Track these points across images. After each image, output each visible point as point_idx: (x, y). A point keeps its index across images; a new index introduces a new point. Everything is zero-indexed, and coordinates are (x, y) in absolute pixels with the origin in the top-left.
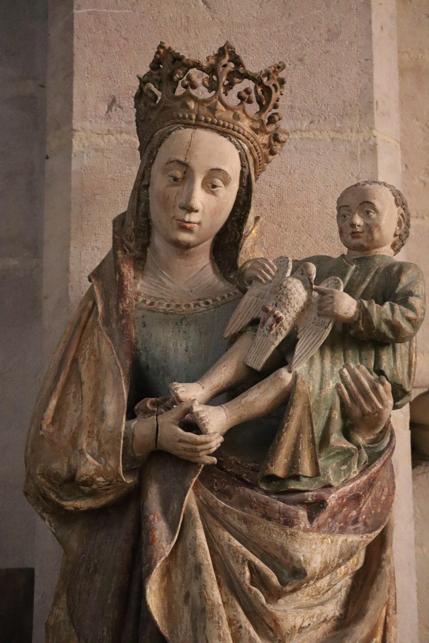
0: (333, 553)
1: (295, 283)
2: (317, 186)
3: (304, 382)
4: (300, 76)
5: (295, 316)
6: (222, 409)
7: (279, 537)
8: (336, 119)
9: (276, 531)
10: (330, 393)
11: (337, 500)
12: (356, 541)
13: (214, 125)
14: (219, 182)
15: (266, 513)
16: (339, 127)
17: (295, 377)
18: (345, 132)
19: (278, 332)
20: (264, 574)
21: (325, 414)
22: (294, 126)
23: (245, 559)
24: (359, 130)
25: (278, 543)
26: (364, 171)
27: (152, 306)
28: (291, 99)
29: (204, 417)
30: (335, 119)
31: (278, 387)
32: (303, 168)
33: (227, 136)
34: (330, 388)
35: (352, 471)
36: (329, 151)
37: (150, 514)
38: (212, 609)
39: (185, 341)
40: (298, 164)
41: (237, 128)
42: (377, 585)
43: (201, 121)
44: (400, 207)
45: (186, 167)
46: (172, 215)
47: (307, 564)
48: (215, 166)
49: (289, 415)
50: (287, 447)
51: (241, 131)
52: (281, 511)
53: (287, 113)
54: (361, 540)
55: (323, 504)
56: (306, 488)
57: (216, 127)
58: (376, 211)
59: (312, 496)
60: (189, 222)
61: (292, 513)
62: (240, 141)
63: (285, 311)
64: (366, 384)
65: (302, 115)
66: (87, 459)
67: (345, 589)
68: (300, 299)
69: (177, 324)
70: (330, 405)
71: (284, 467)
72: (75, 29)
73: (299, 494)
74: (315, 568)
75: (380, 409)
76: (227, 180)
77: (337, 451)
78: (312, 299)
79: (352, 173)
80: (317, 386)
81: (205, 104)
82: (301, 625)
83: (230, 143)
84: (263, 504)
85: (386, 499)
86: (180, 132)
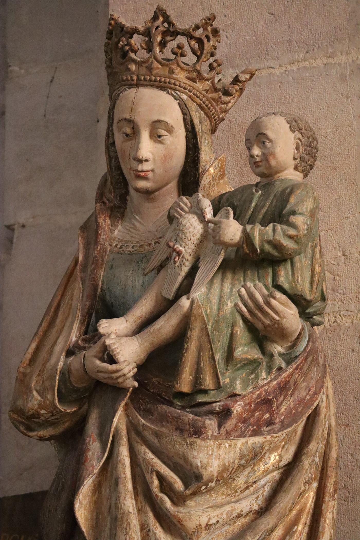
0: (232, 456)
1: (189, 219)
2: (312, 111)
3: (199, 306)
4: (297, 11)
5: (194, 248)
6: (136, 339)
7: (181, 447)
8: (328, 46)
9: (179, 443)
10: (229, 312)
11: (243, 407)
12: (259, 442)
13: (152, 82)
14: (162, 132)
15: (179, 426)
16: (331, 52)
17: (192, 303)
18: (336, 56)
19: (182, 263)
20: (169, 481)
21: (226, 331)
22: (292, 58)
23: (153, 470)
24: (348, 52)
25: (180, 452)
26: (353, 90)
27: (121, 249)
28: (290, 34)
29: (115, 348)
30: (327, 45)
31: (179, 313)
32: (300, 96)
33: (166, 90)
34: (229, 307)
35: (260, 379)
36: (322, 76)
37: (87, 437)
38: (123, 518)
39: (142, 277)
40: (296, 93)
41: (173, 81)
42: (292, 479)
43: (141, 80)
44: (297, 132)
45: (132, 124)
46: (129, 167)
47: (203, 468)
48: (156, 118)
49: (187, 338)
50: (190, 366)
51: (177, 83)
52: (191, 422)
53: (286, 48)
54: (264, 440)
55: (230, 412)
56: (213, 400)
57: (154, 83)
58: (271, 141)
59: (220, 406)
60: (143, 171)
61: (200, 424)
62: (178, 92)
63: (184, 244)
64: (260, 299)
65: (299, 47)
66: (33, 395)
67: (270, 484)
68: (196, 232)
69: (138, 262)
70: (232, 323)
71: (190, 384)
72: (110, 4)
73: (209, 405)
74: (211, 471)
75: (277, 320)
76: (169, 128)
77: (243, 362)
78: (209, 229)
79: (342, 94)
80: (215, 307)
81: (143, 65)
82: (207, 523)
83: (168, 95)
84: (176, 418)
85: (311, 398)
86: (126, 93)
